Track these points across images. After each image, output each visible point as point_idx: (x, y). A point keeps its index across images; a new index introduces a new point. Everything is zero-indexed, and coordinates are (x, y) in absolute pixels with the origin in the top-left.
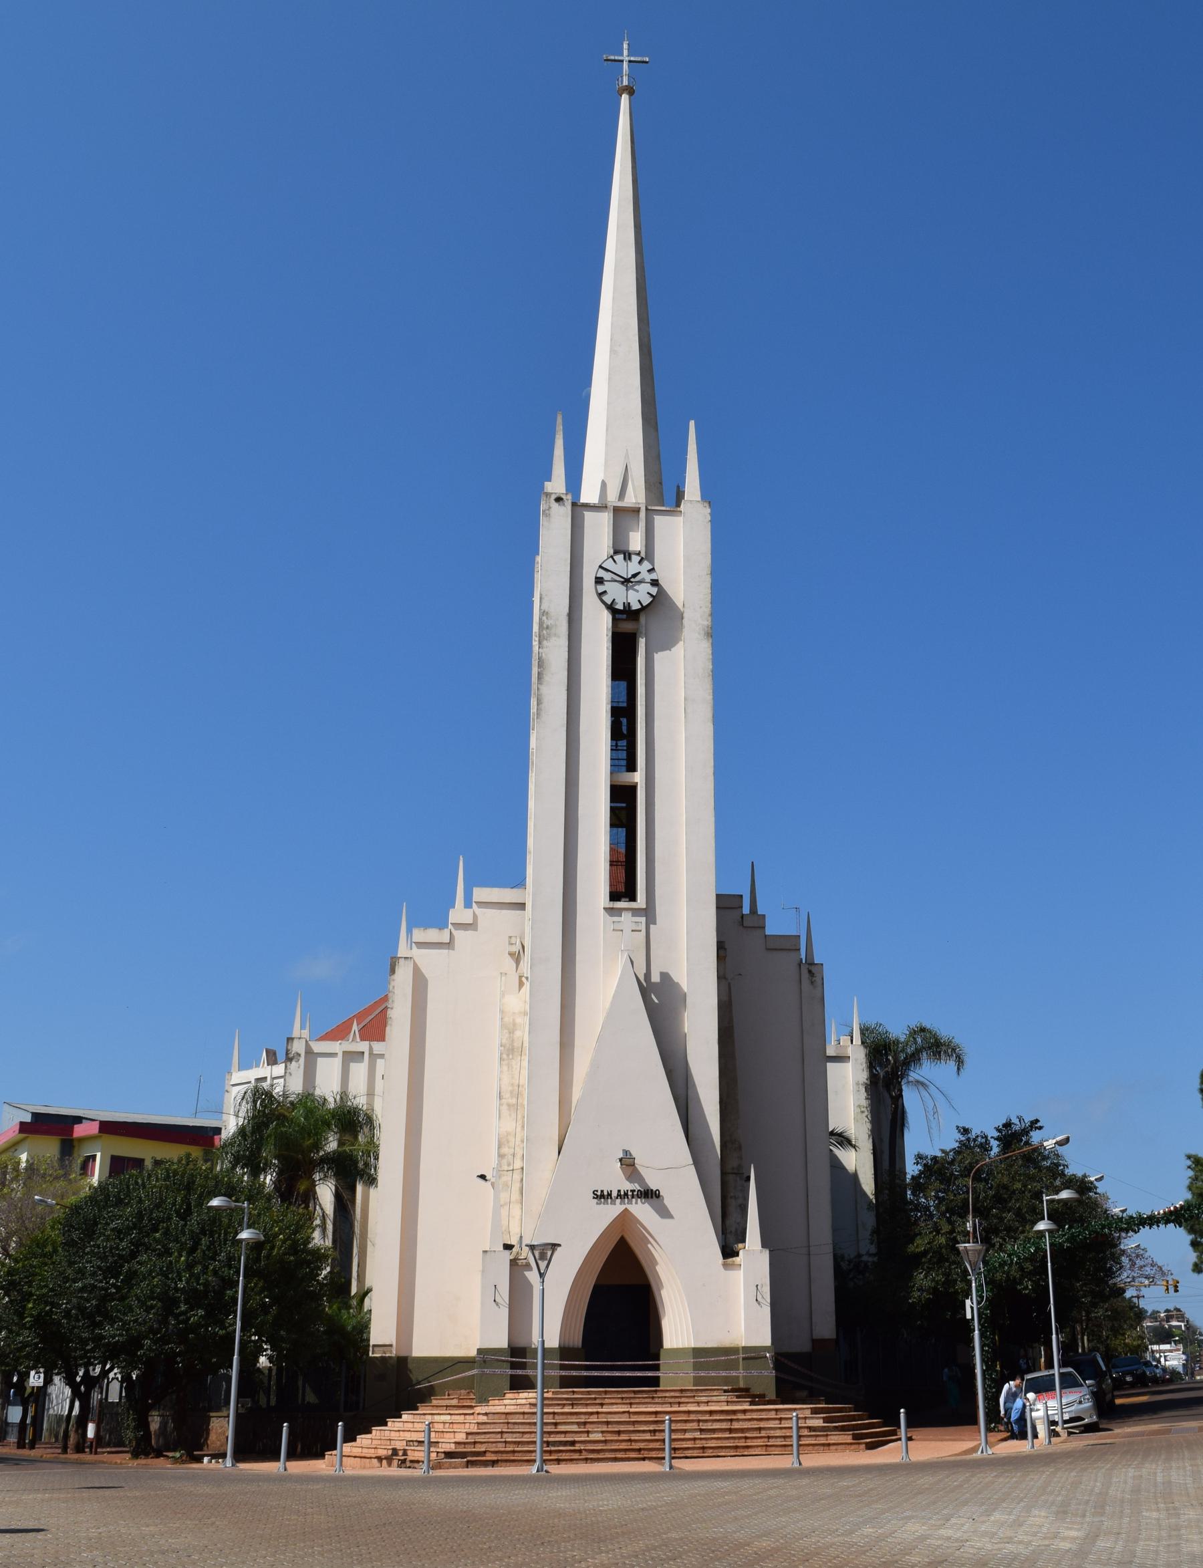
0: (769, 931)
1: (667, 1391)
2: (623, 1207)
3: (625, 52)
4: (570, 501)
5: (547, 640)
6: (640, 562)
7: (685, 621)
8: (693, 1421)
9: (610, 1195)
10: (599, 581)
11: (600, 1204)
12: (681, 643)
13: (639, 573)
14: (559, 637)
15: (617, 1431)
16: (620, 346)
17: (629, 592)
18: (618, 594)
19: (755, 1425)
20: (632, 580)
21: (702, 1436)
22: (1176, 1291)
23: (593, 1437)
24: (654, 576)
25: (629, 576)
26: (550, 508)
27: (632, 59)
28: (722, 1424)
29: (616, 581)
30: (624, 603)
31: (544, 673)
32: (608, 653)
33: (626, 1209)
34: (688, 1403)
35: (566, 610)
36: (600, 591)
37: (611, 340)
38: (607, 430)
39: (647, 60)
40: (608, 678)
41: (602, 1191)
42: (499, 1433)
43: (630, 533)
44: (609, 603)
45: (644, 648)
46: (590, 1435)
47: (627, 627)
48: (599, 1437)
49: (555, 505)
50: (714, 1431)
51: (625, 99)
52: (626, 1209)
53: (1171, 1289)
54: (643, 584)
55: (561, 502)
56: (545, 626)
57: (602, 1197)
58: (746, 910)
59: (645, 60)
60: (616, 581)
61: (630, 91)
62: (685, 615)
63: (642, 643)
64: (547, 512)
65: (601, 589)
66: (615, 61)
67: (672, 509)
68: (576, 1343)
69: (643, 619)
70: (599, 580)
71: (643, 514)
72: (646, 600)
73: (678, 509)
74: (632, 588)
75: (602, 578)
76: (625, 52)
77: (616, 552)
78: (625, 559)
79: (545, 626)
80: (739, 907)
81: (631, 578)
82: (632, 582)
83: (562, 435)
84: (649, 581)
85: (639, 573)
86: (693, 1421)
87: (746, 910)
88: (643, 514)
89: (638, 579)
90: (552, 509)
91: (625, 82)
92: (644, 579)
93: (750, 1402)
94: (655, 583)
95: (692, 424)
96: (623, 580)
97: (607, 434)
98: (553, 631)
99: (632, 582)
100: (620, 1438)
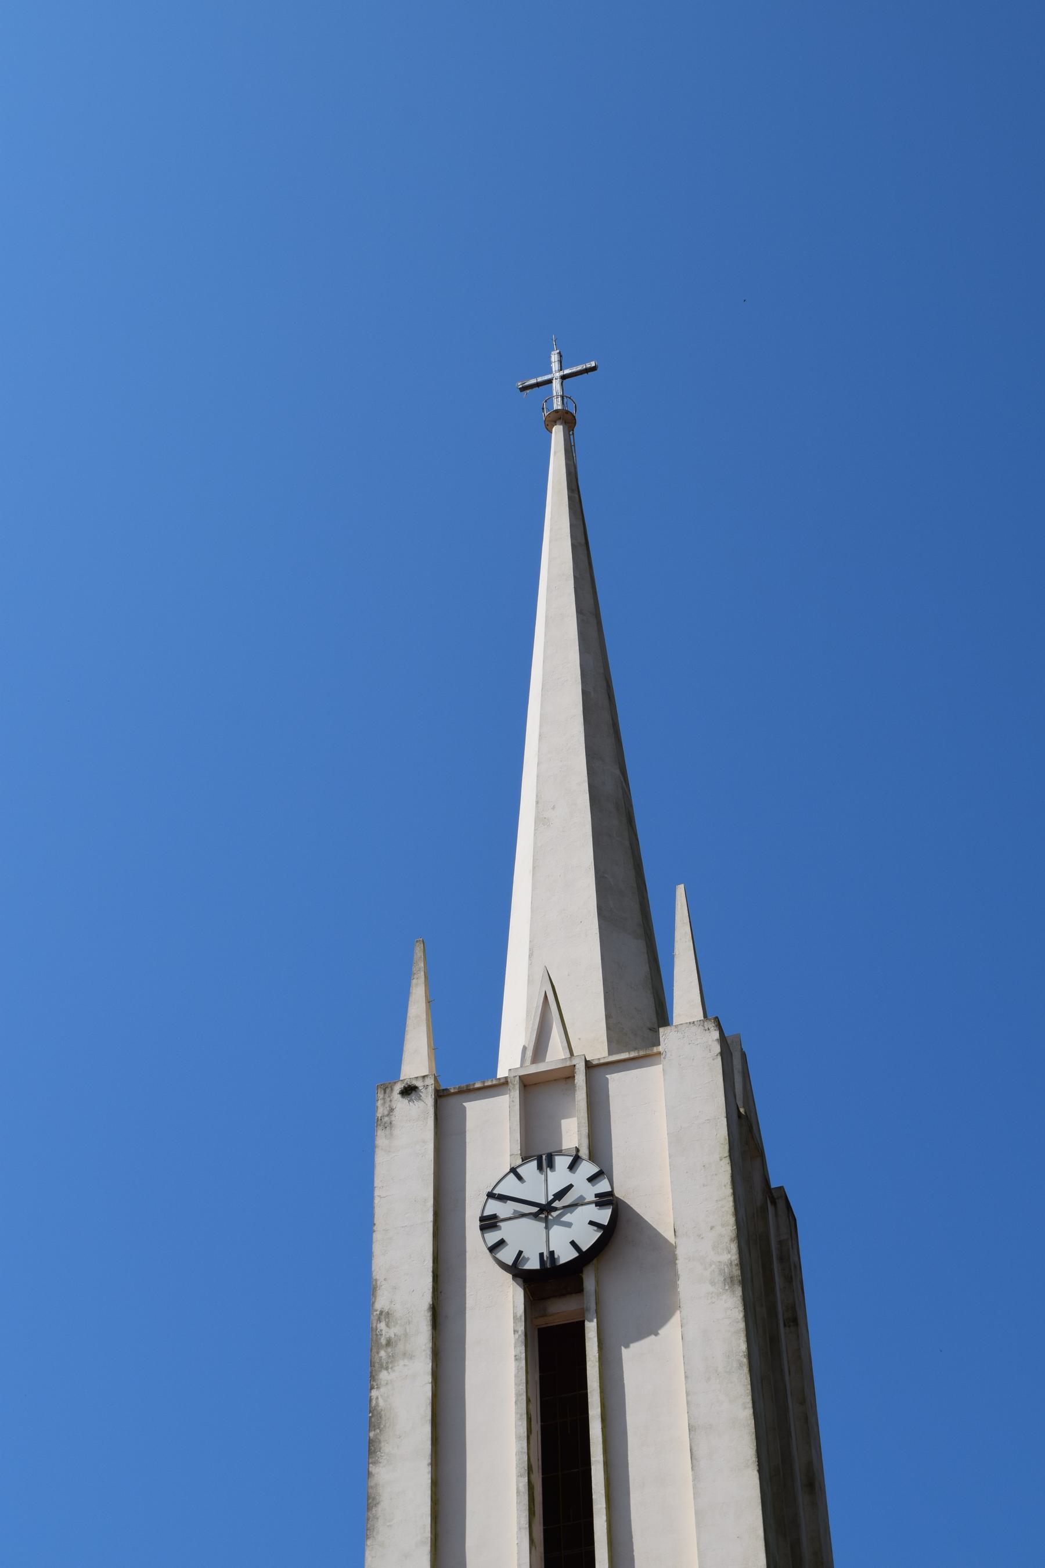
3: (555, 366)
4: (431, 1089)
5: (387, 1369)
6: (572, 1167)
7: (682, 1265)
10: (489, 1223)
12: (676, 1319)
13: (571, 1186)
14: (411, 1357)
16: (553, 808)
17: (551, 1232)
20: (556, 1204)
25: (551, 1197)
26: (392, 1110)
27: (567, 371)
29: (523, 1215)
30: (541, 1255)
31: (382, 1438)
32: (518, 1369)
35: (427, 1299)
37: (537, 802)
38: (531, 956)
39: (593, 364)
40: (521, 1419)
43: (563, 1121)
45: (596, 1339)
47: (561, 1310)
49: (401, 1104)
51: (558, 433)
54: (580, 1209)
55: (413, 1096)
56: (383, 1341)
59: (588, 366)
60: (523, 1215)
61: (567, 419)
62: (680, 1252)
63: (591, 1329)
64: (386, 1119)
65: (493, 1237)
66: (538, 385)
67: (642, 1053)
69: (589, 1283)
71: (580, 1078)
72: (588, 1238)
73: (655, 1049)
74: (558, 1221)
76: (555, 366)
77: (525, 1159)
78: (540, 1167)
79: (383, 1341)
81: (553, 1201)
82: (556, 1209)
83: (422, 979)
84: (593, 1199)
85: (571, 1186)
88: (580, 1078)
89: (567, 1200)
90: (396, 1112)
91: (557, 405)
92: (582, 1197)
94: (605, 1200)
95: (680, 890)
96: (535, 1209)
97: (530, 964)
98: (401, 1347)
99: (556, 1209)
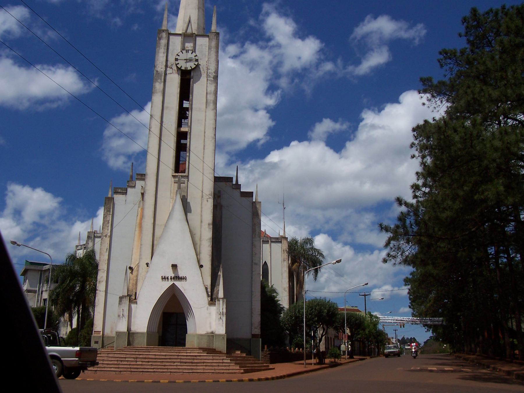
0: (242, 190)
1: (138, 347)
2: (172, 283)
6: (192, 53)
8: (179, 359)
9: (168, 278)
11: (163, 281)
15: (185, 362)
18: (183, 65)
19: (203, 361)
21: (181, 364)
22: (404, 327)
23: (138, 363)
24: (197, 58)
28: (190, 360)
30: (185, 67)
33: (174, 283)
34: (182, 352)
36: (176, 63)
41: (165, 276)
42: (116, 361)
44: (180, 67)
46: (137, 362)
48: (141, 363)
50: (186, 363)
52: (174, 283)
53: (402, 327)
57: (164, 278)
58: (234, 182)
65: (177, 62)
68: (154, 331)
70: (176, 59)
72: (193, 66)
75: (178, 59)
78: (186, 52)
80: (184, 164)
86: (179, 359)
87: (234, 182)
93: (207, 353)
100: (223, 365)
